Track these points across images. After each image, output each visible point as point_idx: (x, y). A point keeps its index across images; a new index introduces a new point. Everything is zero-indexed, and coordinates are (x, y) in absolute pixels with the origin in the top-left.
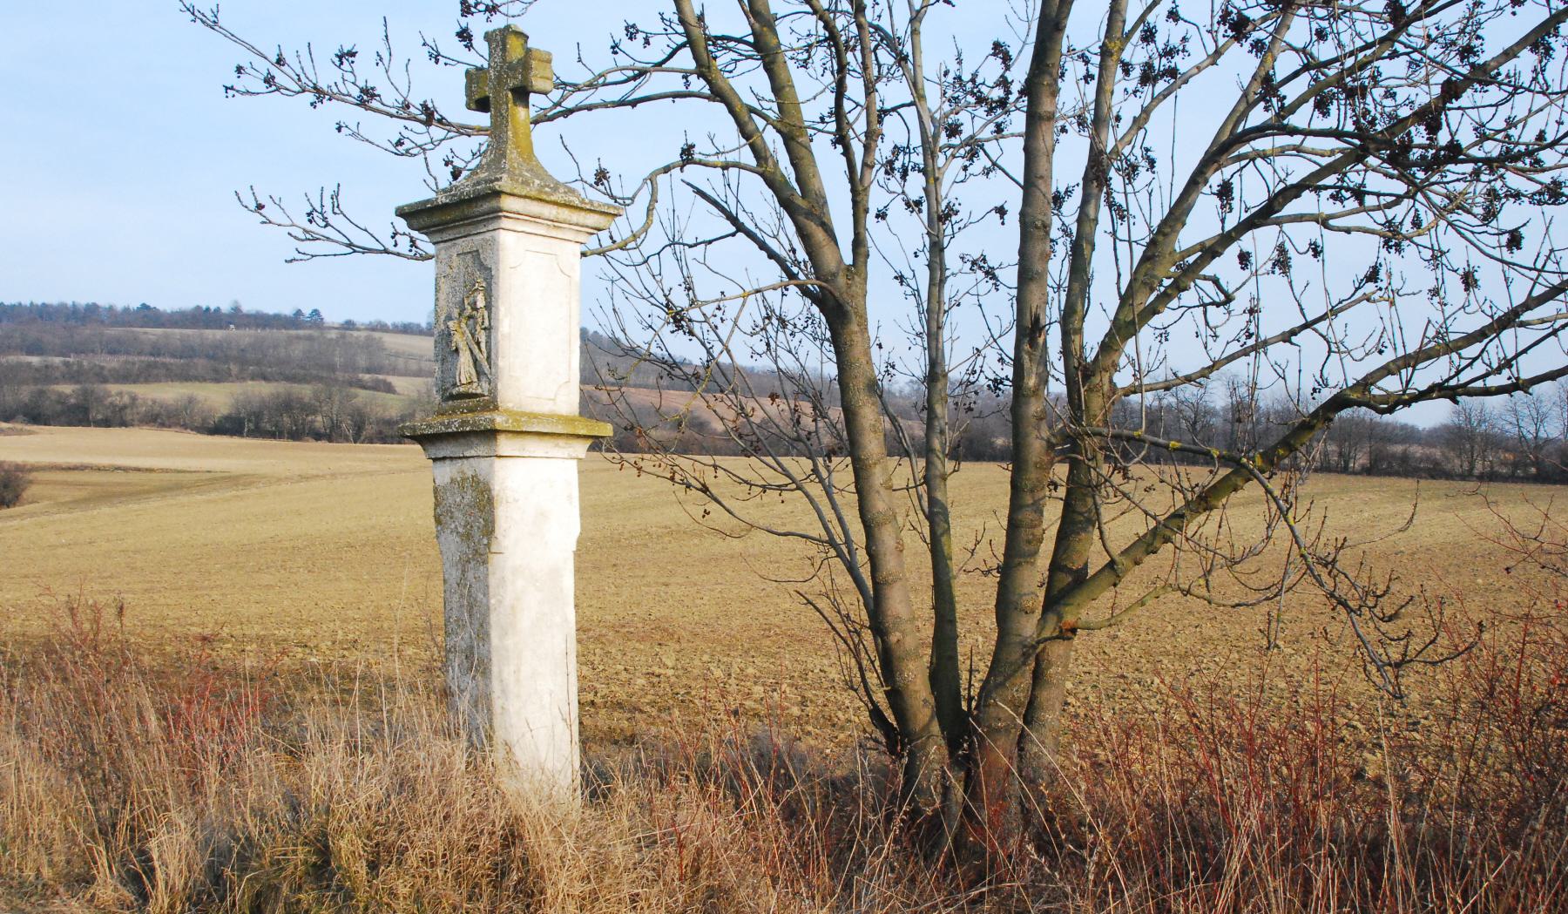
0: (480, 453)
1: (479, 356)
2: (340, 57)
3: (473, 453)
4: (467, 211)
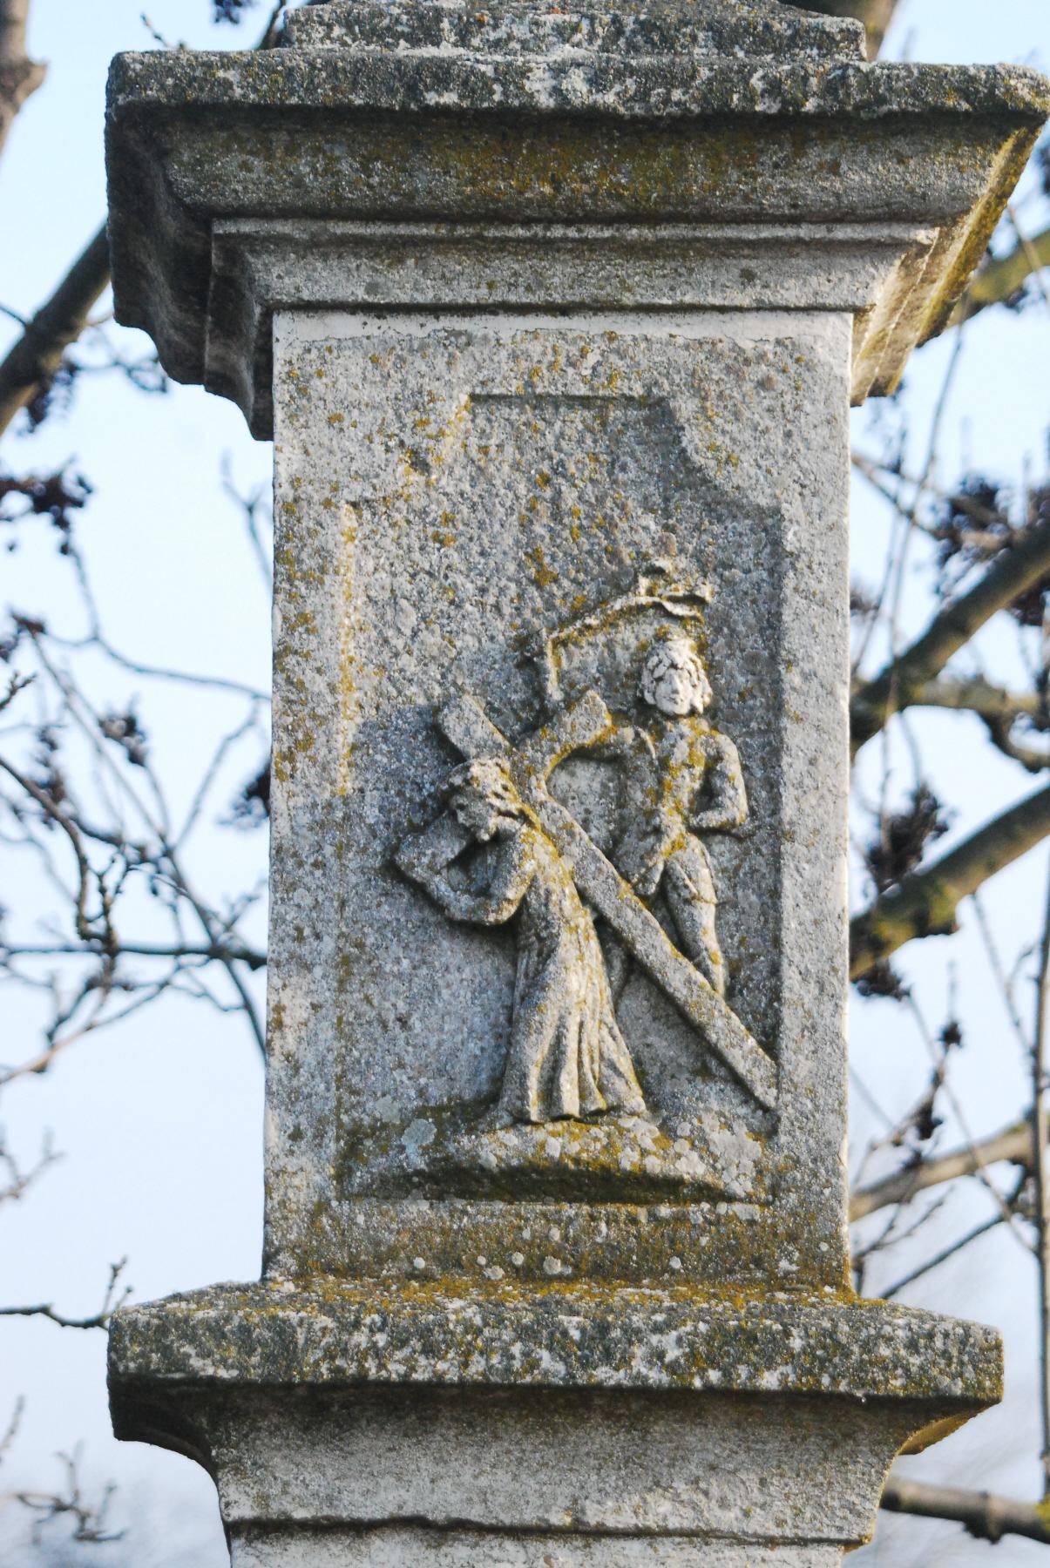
0: (728, 1519)
1: (677, 975)
3: (662, 1510)
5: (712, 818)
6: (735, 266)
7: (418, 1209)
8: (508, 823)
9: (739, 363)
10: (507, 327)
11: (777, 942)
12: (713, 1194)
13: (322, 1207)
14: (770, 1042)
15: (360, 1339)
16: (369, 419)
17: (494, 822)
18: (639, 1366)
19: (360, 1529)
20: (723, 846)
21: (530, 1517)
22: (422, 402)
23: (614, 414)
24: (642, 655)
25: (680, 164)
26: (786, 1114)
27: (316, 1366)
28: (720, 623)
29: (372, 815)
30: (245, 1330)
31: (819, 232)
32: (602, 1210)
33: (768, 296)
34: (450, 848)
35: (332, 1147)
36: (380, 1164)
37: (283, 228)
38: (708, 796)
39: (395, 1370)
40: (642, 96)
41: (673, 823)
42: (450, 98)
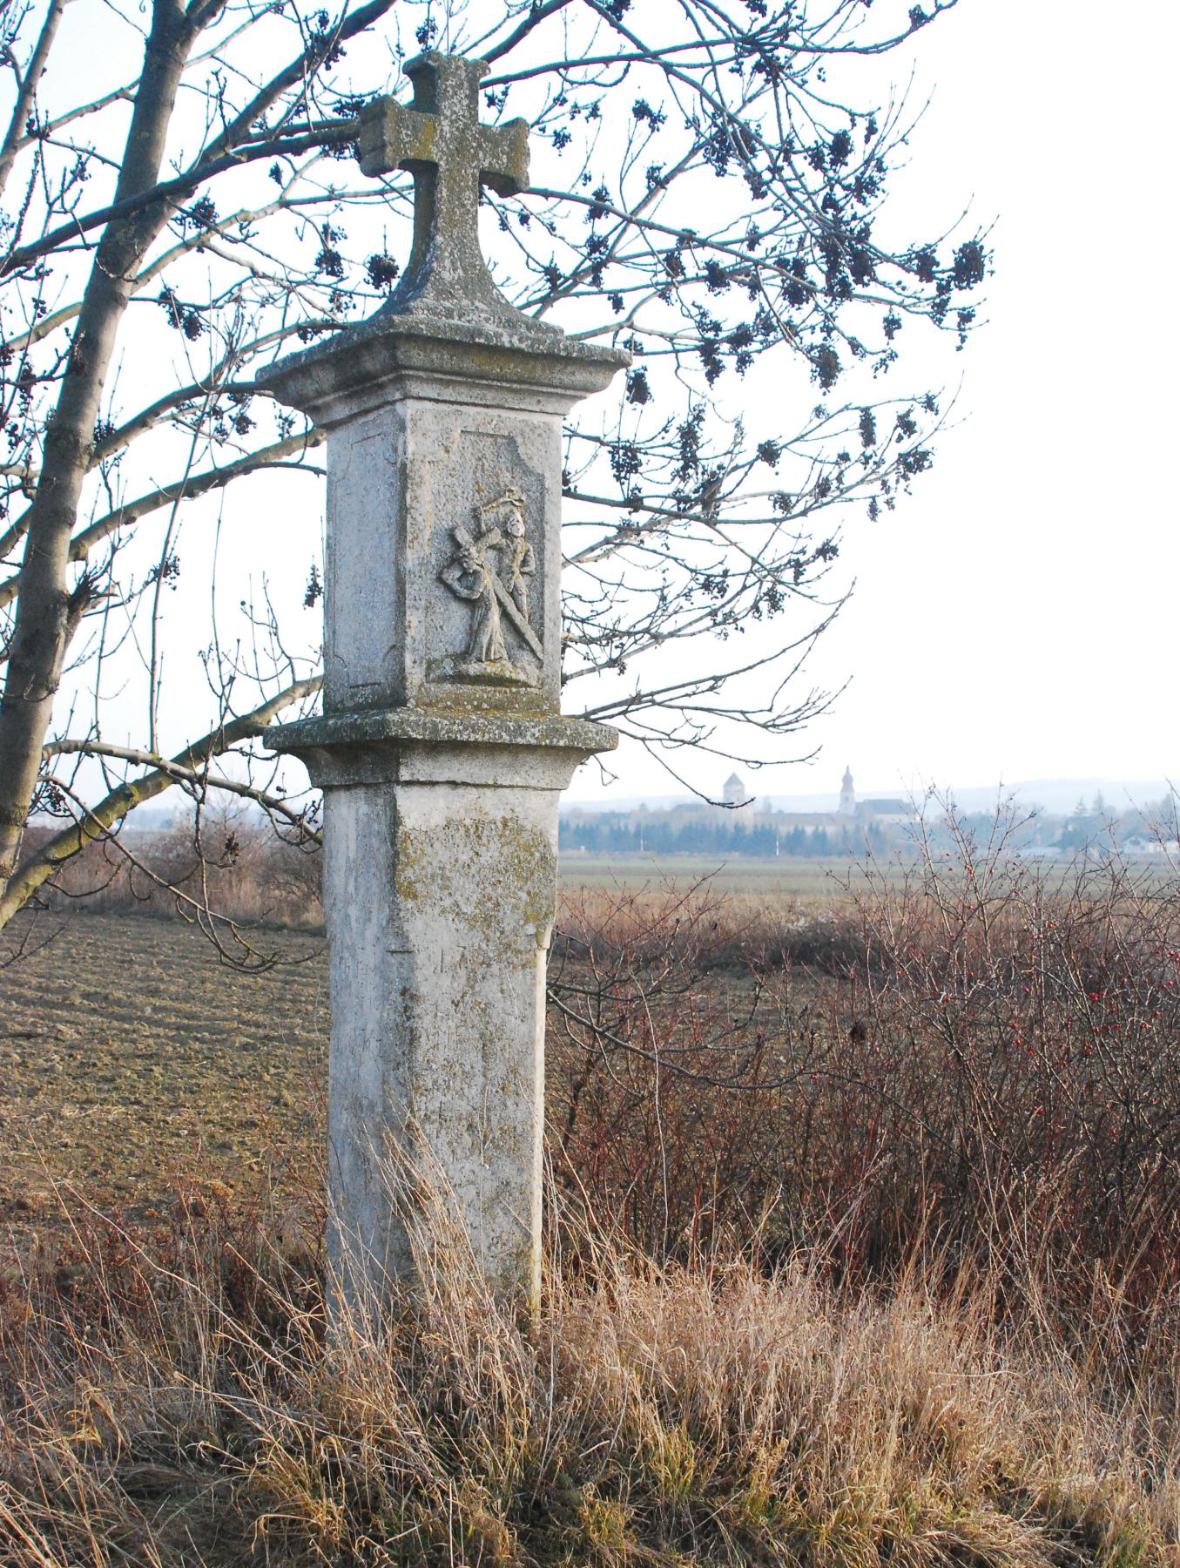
0: (533, 783)
1: (518, 618)
2: (819, 78)
3: (518, 780)
4: (539, 372)
5: (526, 569)
6: (536, 399)
7: (448, 686)
8: (478, 568)
9: (534, 428)
10: (472, 410)
11: (542, 609)
12: (526, 685)
13: (422, 685)
14: (541, 638)
15: (455, 727)
16: (434, 436)
17: (475, 567)
18: (528, 738)
19: (433, 784)
20: (527, 577)
21: (483, 782)
22: (448, 431)
23: (499, 440)
24: (507, 518)
25: (534, 367)
26: (545, 661)
27: (443, 735)
28: (527, 508)
29: (434, 562)
30: (425, 724)
31: (563, 392)
32: (498, 689)
33: (544, 409)
34: (458, 574)
35: (424, 666)
36: (438, 672)
37: (421, 374)
38: (524, 563)
39: (465, 737)
40: (532, 346)
41: (517, 570)
42: (482, 341)
